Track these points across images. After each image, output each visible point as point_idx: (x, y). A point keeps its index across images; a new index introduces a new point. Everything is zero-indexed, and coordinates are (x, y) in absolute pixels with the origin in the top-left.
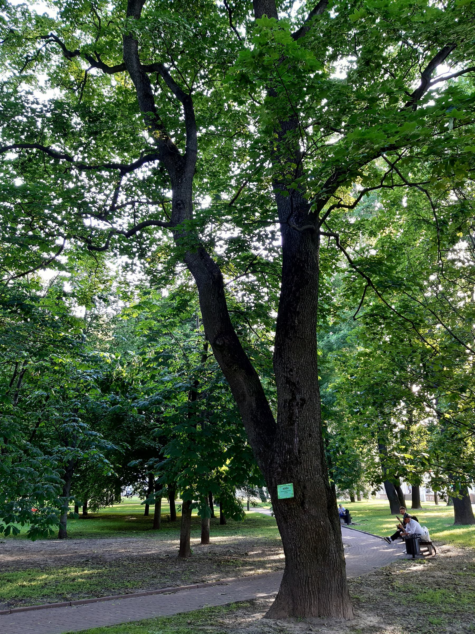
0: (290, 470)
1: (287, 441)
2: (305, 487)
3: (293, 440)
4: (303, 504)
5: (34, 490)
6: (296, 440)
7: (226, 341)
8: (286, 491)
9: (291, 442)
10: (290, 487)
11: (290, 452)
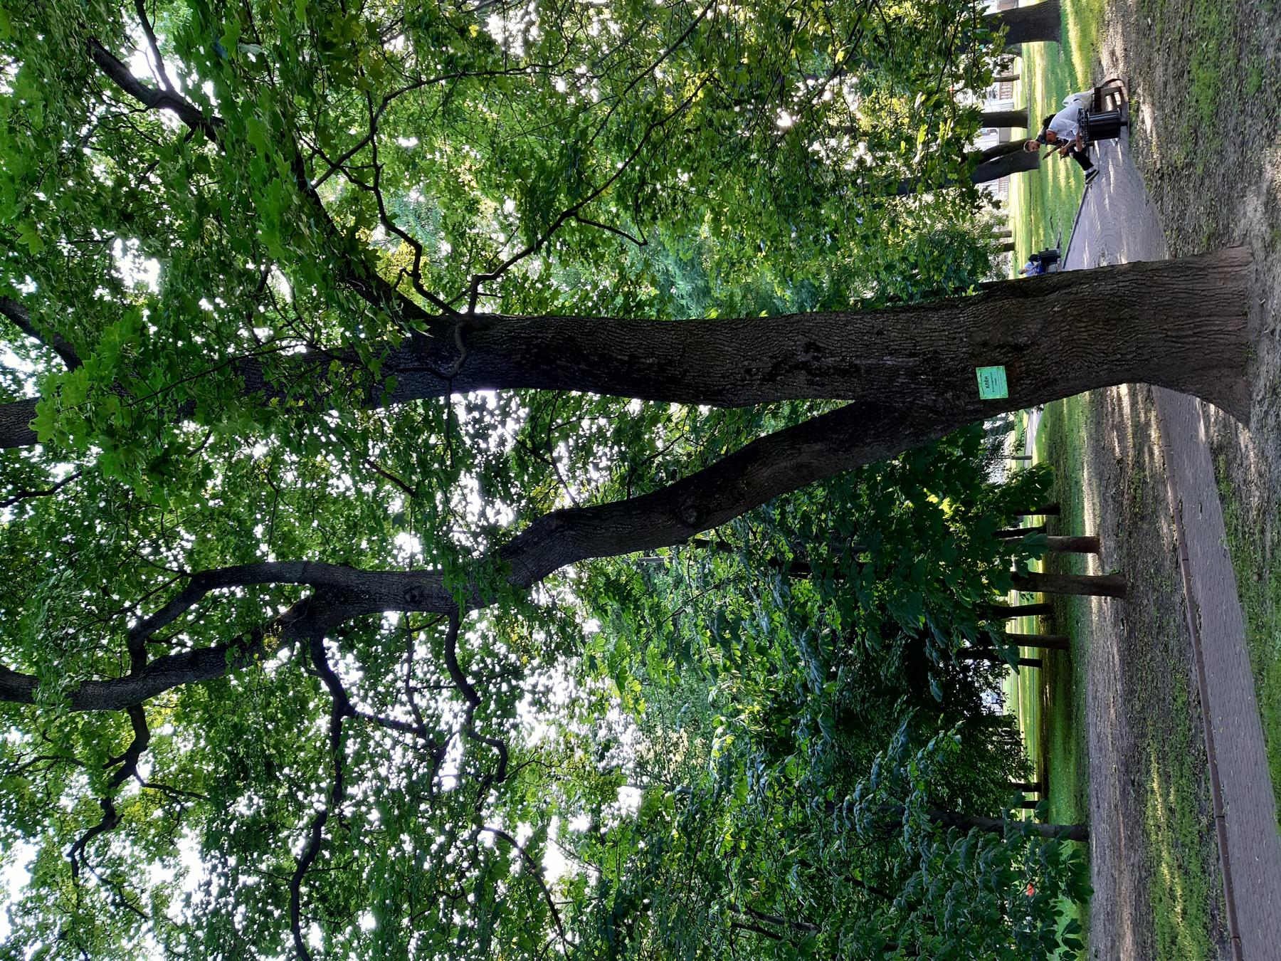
0: (949, 373)
1: (891, 380)
2: (985, 344)
3: (890, 368)
4: (1018, 348)
5: (991, 890)
6: (889, 361)
7: (689, 502)
8: (992, 382)
9: (894, 372)
10: (983, 373)
11: (912, 374)
